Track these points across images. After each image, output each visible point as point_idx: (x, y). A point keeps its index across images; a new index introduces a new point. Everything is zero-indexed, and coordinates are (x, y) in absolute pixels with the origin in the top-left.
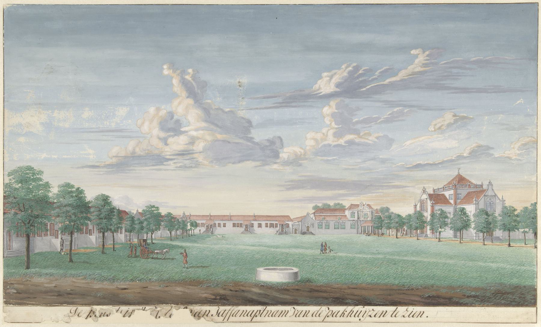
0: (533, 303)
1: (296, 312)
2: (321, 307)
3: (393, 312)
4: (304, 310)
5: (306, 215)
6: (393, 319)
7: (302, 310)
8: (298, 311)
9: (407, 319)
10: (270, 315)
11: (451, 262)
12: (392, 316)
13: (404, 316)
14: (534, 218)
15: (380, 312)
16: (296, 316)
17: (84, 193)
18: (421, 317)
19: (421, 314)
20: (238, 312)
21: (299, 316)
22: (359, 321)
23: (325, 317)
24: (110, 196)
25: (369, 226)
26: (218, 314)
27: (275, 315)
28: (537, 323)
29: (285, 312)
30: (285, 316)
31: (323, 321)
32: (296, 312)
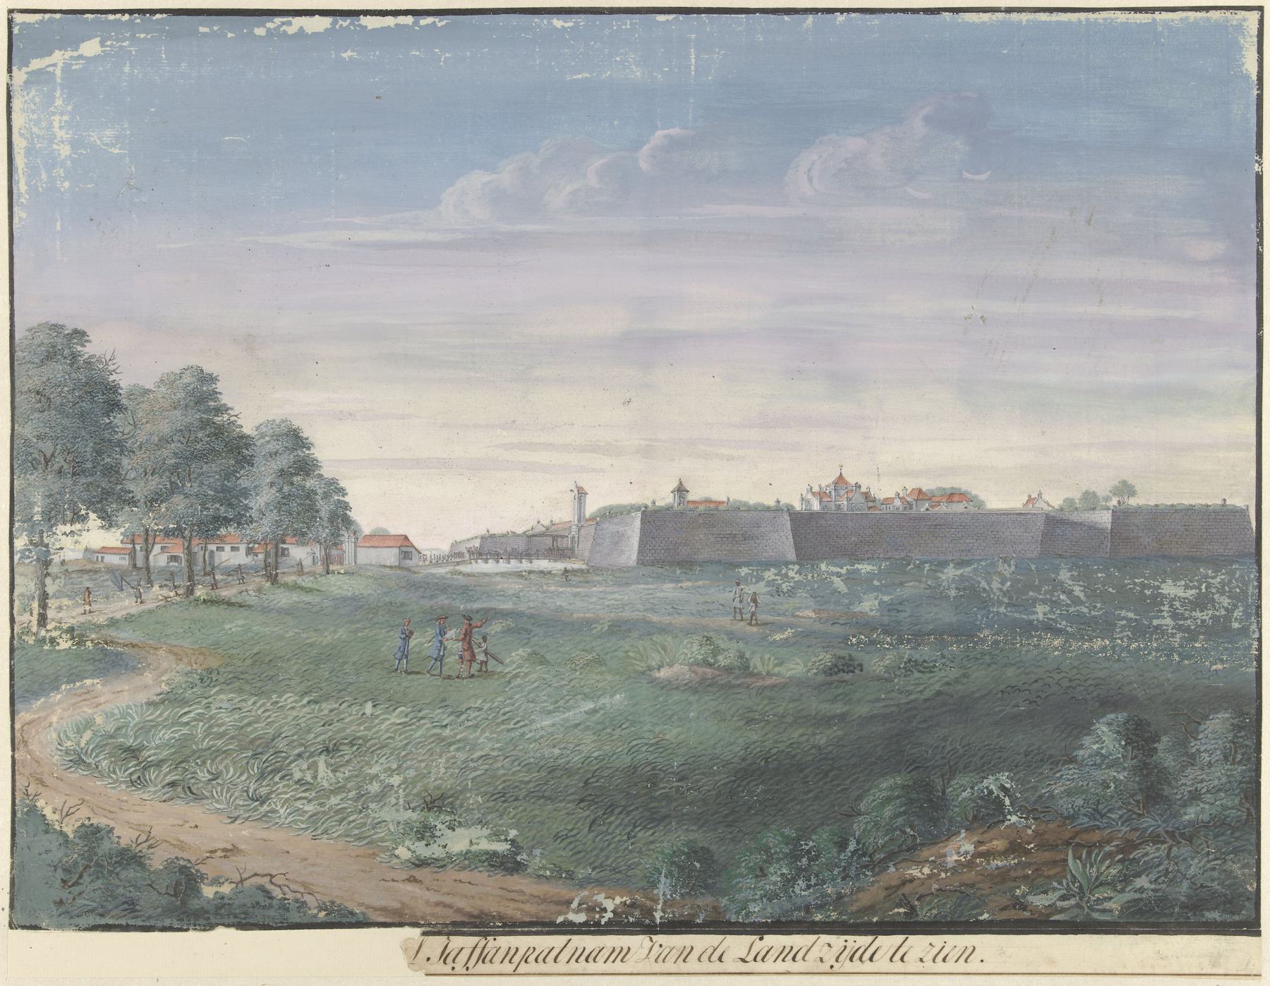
0: (1251, 927)
2: (568, 937)
3: (471, 950)
5: (367, 530)
6: (898, 966)
10: (583, 958)
11: (186, 709)
13: (921, 960)
15: (957, 949)
23: (519, 963)
24: (102, 531)
26: (444, 956)
27: (492, 959)
29: (613, 951)
30: (966, 961)
31: (515, 973)
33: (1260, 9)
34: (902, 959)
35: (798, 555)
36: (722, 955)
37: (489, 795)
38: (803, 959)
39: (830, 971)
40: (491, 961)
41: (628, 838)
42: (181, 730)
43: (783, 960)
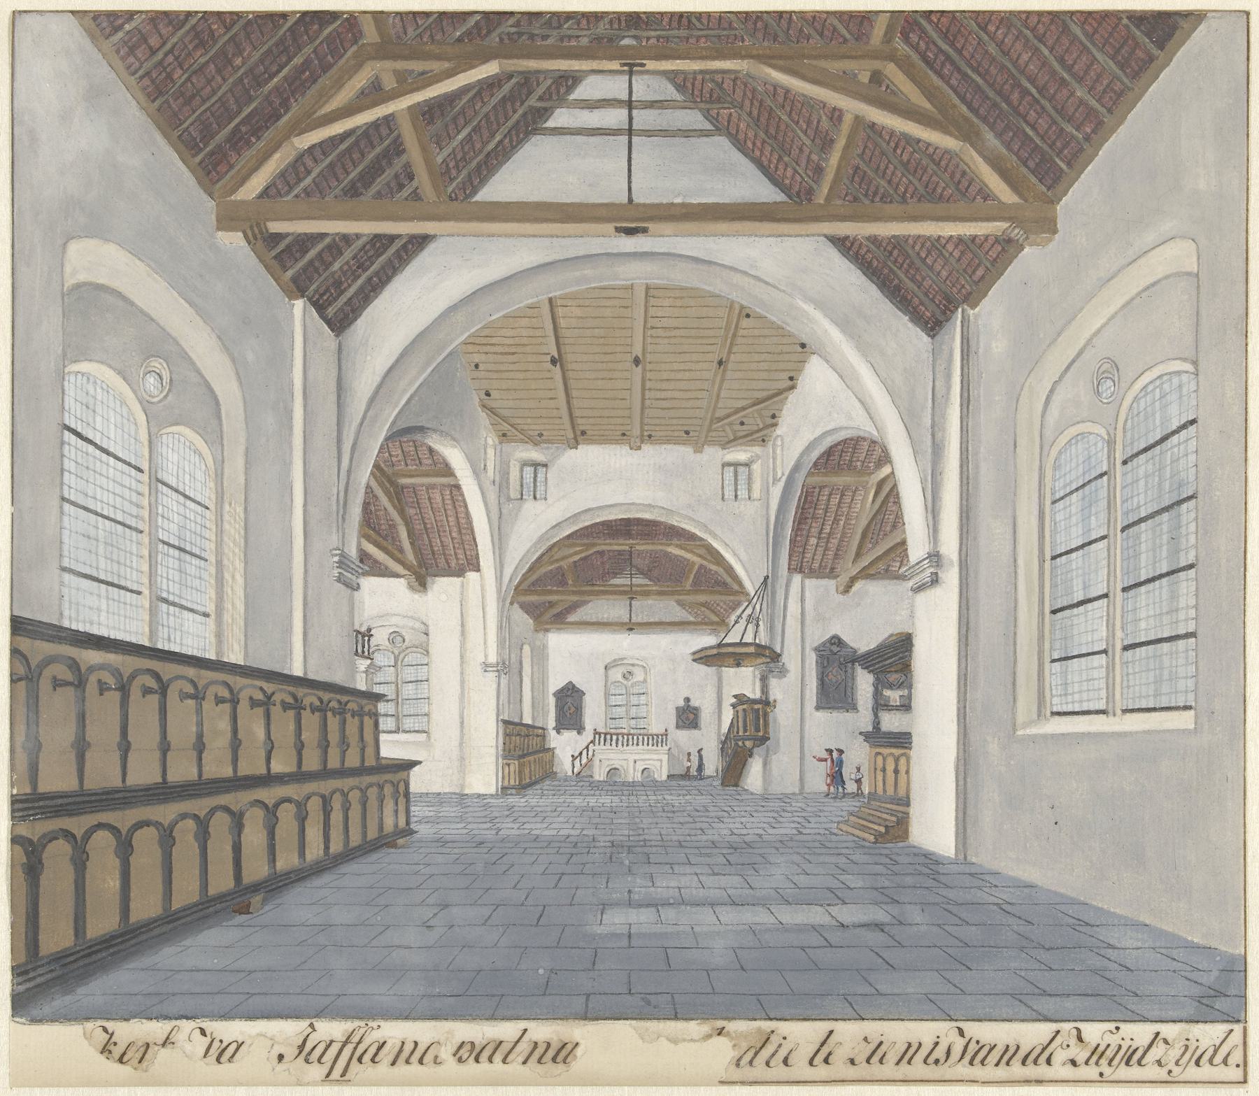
1: (973, 1047)
4: (998, 1043)
6: (822, 1071)
7: (328, 1039)
8: (980, 1045)
9: (862, 1070)
12: (815, 1063)
13: (852, 1062)
14: (627, 675)
16: (218, 1060)
17: (492, 676)
18: (909, 1063)
19: (562, 1053)
20: (326, 1050)
21: (982, 1062)
22: (1100, 1079)
25: (611, 735)
28: (1245, 1082)
32: (973, 1047)
33: (16, 14)
34: (826, 1061)
35: (885, 463)
36: (1228, 1054)
37: (585, 753)
38: (373, 1060)
39: (1100, 1079)
40: (1139, 1063)
41: (526, 849)
42: (594, 545)
43: (539, 1061)
